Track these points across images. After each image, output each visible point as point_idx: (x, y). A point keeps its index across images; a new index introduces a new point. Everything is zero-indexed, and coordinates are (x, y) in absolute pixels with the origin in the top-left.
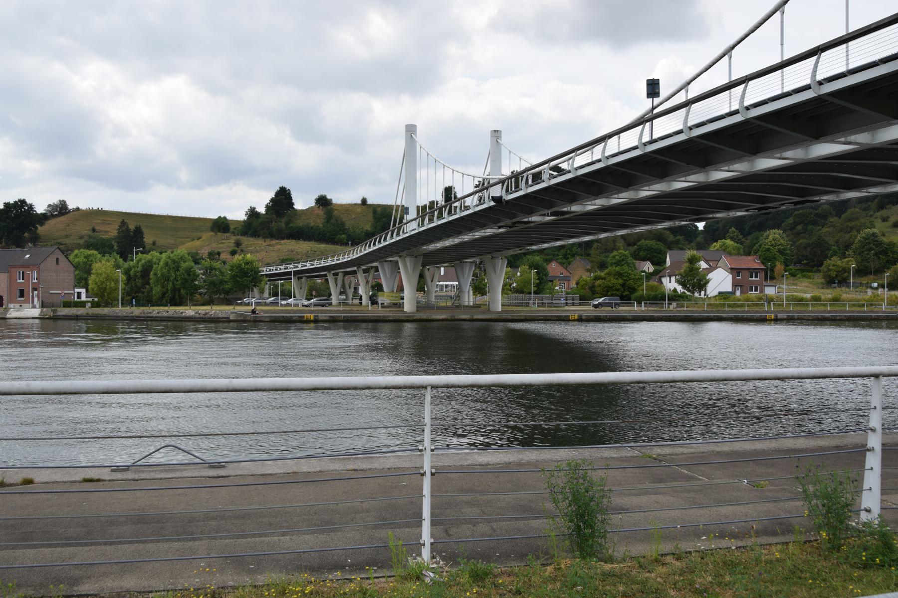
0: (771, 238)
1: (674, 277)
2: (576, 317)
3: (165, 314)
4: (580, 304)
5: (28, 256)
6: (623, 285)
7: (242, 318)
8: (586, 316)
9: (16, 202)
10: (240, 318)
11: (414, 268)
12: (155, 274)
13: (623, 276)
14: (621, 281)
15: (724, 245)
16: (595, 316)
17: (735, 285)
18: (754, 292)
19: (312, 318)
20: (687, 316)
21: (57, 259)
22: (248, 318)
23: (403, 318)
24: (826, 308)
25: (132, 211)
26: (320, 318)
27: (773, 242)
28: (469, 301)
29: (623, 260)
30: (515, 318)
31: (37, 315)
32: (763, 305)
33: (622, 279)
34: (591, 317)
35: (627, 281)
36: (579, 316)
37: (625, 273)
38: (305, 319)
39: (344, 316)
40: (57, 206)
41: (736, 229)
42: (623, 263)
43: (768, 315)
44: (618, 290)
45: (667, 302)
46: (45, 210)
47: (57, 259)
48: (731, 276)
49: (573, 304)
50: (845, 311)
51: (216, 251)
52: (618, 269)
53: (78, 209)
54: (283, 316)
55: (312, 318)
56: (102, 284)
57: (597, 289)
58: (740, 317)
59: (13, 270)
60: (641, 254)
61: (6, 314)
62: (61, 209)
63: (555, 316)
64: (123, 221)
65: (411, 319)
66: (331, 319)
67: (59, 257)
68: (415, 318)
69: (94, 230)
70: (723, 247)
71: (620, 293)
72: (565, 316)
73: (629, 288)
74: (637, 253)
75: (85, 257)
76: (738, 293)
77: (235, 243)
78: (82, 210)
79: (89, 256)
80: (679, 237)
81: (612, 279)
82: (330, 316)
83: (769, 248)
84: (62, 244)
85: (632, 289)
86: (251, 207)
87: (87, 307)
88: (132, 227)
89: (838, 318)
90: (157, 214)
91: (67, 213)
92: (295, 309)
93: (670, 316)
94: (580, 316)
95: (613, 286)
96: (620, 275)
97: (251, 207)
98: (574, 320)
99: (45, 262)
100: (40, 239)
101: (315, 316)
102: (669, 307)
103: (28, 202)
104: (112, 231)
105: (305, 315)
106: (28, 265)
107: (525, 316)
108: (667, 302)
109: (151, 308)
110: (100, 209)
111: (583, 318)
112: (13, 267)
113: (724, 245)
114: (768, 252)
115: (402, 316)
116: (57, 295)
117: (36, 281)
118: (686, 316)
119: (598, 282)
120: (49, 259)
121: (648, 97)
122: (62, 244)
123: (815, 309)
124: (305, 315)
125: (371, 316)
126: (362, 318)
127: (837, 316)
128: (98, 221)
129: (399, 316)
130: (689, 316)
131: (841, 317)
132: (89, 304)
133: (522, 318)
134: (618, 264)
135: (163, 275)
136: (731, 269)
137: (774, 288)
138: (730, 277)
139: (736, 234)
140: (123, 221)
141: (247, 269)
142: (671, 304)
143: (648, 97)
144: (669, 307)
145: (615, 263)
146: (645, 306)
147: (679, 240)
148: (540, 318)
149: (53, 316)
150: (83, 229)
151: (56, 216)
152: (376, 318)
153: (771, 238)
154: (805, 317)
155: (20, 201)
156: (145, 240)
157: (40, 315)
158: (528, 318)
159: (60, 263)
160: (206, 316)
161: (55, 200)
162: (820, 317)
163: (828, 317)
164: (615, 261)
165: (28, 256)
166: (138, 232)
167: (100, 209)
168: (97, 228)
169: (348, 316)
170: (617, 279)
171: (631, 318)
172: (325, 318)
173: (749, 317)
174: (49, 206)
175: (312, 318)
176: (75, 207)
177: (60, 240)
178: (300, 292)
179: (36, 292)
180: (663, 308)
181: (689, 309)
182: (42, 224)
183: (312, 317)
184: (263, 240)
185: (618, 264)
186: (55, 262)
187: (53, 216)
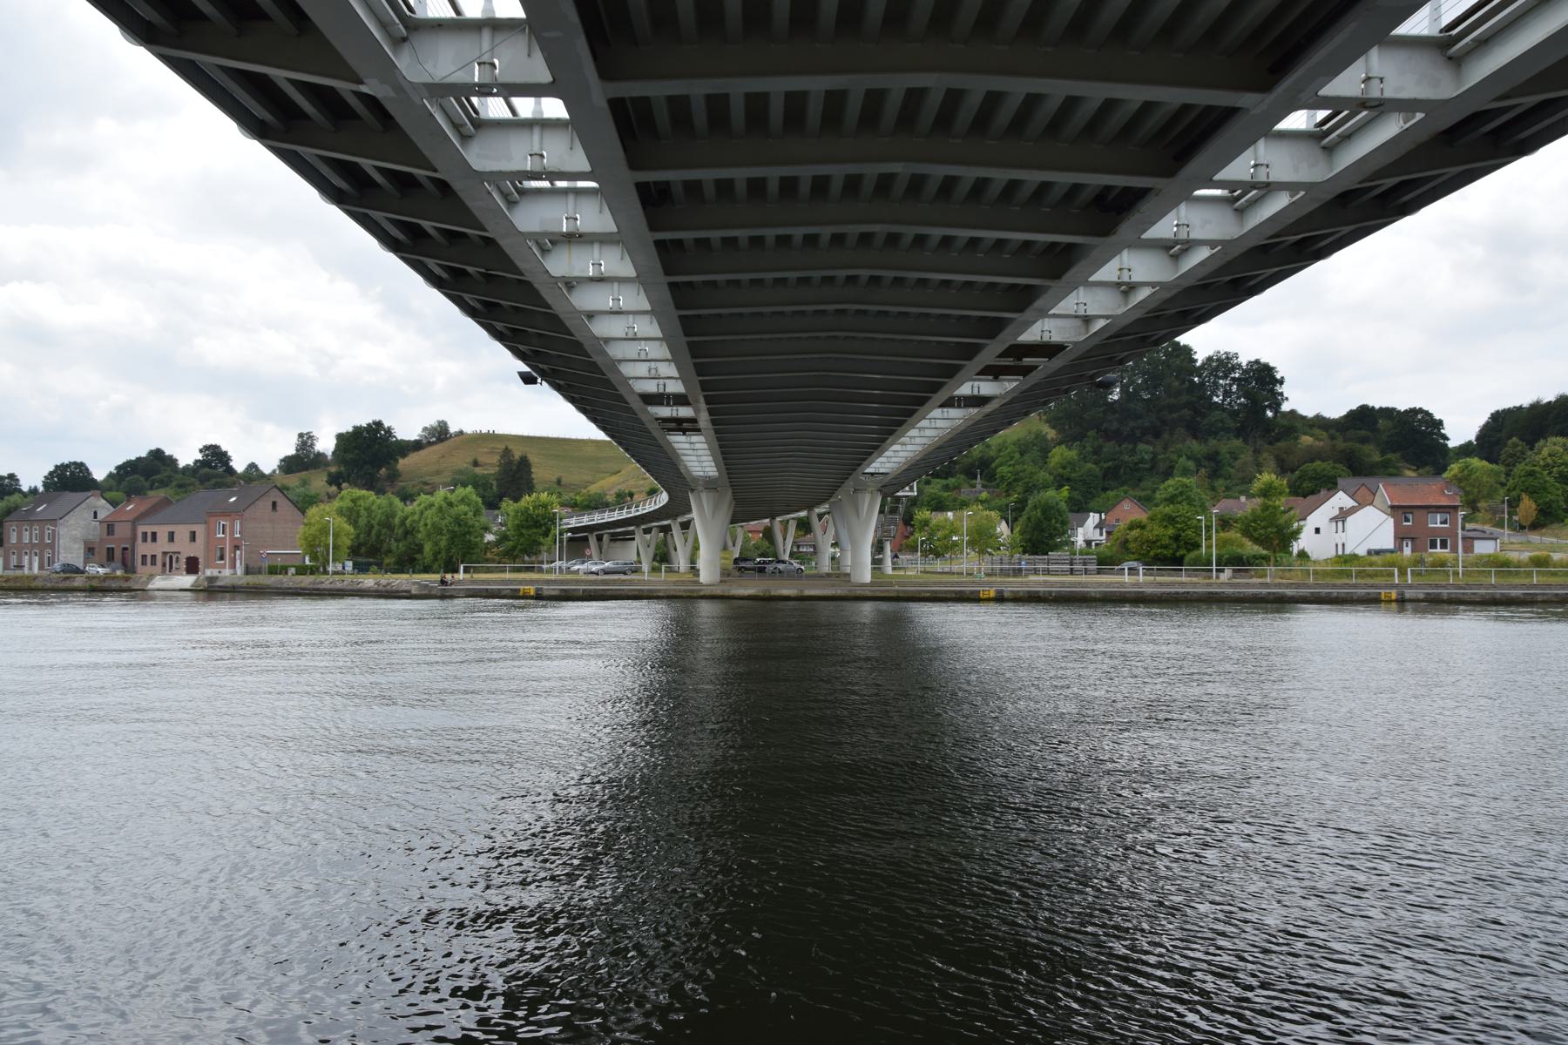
0: (1545, 452)
1: (1097, 515)
2: (992, 594)
4: (1099, 572)
5: (233, 499)
6: (1176, 538)
7: (426, 592)
8: (1011, 591)
9: (369, 425)
10: (423, 592)
11: (716, 508)
12: (426, 525)
13: (1177, 523)
14: (1171, 531)
15: (1467, 467)
16: (1029, 592)
17: (1400, 537)
18: (1439, 550)
19: (532, 593)
20: (1212, 593)
21: (274, 504)
22: (434, 592)
24: (1488, 579)
25: (538, 434)
26: (546, 593)
27: (1549, 460)
29: (1181, 494)
31: (188, 586)
32: (1391, 575)
33: (1174, 527)
34: (1021, 594)
35: (1184, 531)
37: (1181, 516)
38: (521, 593)
39: (584, 590)
40: (435, 429)
41: (1521, 439)
42: (1180, 499)
43: (1383, 591)
44: (1166, 547)
45: (1214, 567)
46: (419, 435)
47: (274, 504)
48: (1391, 521)
49: (1086, 572)
50: (1308, 586)
51: (627, 491)
52: (1168, 509)
53: (461, 433)
54: (1557, 594)
55: (532, 593)
56: (314, 540)
57: (1132, 546)
58: (1323, 595)
59: (212, 519)
60: (1305, 485)
61: (148, 583)
62: (440, 433)
63: (953, 591)
64: (507, 449)
68: (702, 593)
69: (476, 464)
70: (1466, 472)
71: (1171, 551)
72: (972, 592)
73: (1186, 543)
74: (1298, 483)
75: (353, 501)
76: (1407, 551)
78: (467, 434)
79: (359, 498)
80: (1389, 456)
81: (1156, 527)
83: (1533, 471)
84: (428, 484)
85: (1192, 544)
87: (290, 574)
88: (517, 455)
89: (1540, 598)
90: (573, 437)
91: (446, 439)
92: (970, 579)
93: (1177, 593)
95: (1157, 541)
96: (1171, 520)
98: (989, 600)
100: (400, 476)
101: (537, 590)
102: (1218, 577)
103: (386, 425)
104: (491, 465)
105: (521, 587)
106: (229, 512)
107: (898, 591)
109: (414, 576)
111: (1006, 595)
112: (211, 515)
113: (1467, 467)
114: (1531, 479)
115: (679, 590)
117: (238, 536)
118: (1209, 593)
119: (1136, 533)
120: (260, 503)
122: (428, 484)
123: (1502, 581)
124: (521, 587)
127: (1537, 594)
128: (485, 450)
130: (1216, 593)
131: (1545, 598)
132: (293, 570)
133: (891, 595)
134: (1171, 500)
135: (433, 524)
136: (1392, 507)
137: (1494, 542)
138: (1389, 524)
139: (1519, 448)
140: (507, 449)
142: (1223, 571)
144: (1218, 577)
145: (1166, 500)
146: (1144, 574)
147: (1390, 460)
148: (923, 595)
150: (461, 461)
151: (434, 443)
153: (1545, 452)
154: (1466, 598)
155: (375, 423)
156: (533, 476)
157: (192, 586)
158: (901, 595)
159: (278, 508)
160: (389, 588)
161: (431, 421)
162: (1498, 596)
163: (1517, 598)
164: (1168, 496)
165: (233, 499)
166: (524, 463)
168: (480, 459)
169: (590, 590)
170: (1166, 527)
171: (1098, 596)
172: (554, 593)
173: (1343, 595)
174: (425, 429)
175: (532, 593)
176: (457, 430)
177: (427, 479)
178: (646, 552)
179: (238, 552)
180: (1211, 577)
181: (1359, 581)
182: (404, 456)
183: (532, 590)
185: (1171, 500)
186: (271, 507)
187: (430, 444)
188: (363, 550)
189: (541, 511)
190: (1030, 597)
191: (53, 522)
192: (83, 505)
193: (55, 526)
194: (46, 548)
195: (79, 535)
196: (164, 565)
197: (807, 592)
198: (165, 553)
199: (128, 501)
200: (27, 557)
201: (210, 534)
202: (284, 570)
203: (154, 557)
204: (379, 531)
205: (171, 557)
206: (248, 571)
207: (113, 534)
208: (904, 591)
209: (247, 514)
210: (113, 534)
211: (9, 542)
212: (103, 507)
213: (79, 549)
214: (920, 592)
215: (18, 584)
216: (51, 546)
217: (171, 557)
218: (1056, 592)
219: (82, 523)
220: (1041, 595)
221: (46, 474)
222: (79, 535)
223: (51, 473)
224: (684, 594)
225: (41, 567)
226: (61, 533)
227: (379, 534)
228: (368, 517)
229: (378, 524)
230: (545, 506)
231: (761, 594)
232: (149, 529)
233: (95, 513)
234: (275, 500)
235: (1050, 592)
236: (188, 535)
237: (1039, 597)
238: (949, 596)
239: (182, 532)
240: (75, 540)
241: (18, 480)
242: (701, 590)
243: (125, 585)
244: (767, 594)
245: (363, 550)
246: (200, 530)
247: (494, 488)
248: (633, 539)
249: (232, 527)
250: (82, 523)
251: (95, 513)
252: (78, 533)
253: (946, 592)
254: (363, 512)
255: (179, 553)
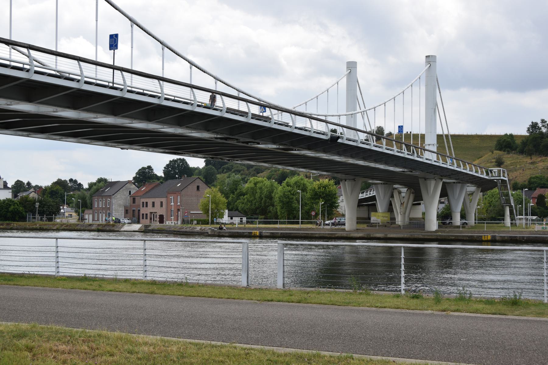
2: (489, 238)
3: (188, 230)
8: (501, 236)
16: (510, 237)
19: (258, 234)
21: (198, 188)
23: (326, 236)
26: (264, 234)
28: (102, 220)
30: (426, 237)
31: (137, 229)
34: (506, 238)
36: (493, 237)
39: (281, 233)
47: (198, 188)
54: (238, 232)
61: (121, 228)
63: (467, 236)
65: (333, 236)
66: (272, 235)
67: (200, 185)
68: (337, 236)
77: (496, 162)
82: (271, 233)
86: (532, 123)
87: (194, 224)
94: (493, 237)
97: (532, 123)
99: (186, 188)
101: (260, 233)
105: (253, 231)
108: (300, 220)
110: (409, 133)
111: (497, 238)
115: (326, 234)
116: (197, 214)
121: (110, 49)
125: (302, 233)
126: (295, 235)
129: (323, 233)
132: (195, 222)
141: (320, 192)
143: (110, 49)
149: (145, 230)
152: (305, 235)
157: (139, 229)
159: (200, 189)
167: (409, 133)
175: (258, 234)
184: (530, 157)
188: (258, 211)
189: (322, 190)
190: (511, 240)
191: (110, 196)
192: (124, 188)
193: (111, 199)
194: (108, 211)
195: (122, 204)
196: (151, 219)
197: (390, 236)
198: (151, 213)
199: (144, 185)
200: (101, 214)
201: (168, 203)
202: (191, 222)
203: (147, 214)
204: (266, 200)
205: (154, 214)
206: (184, 222)
207: (135, 203)
208: (320, 234)
209: (183, 192)
210: (135, 203)
211: (94, 207)
212: (134, 189)
213: (122, 210)
214: (449, 236)
215: (70, 228)
216: (109, 209)
217: (154, 214)
218: (527, 237)
219: (123, 197)
220: (518, 238)
221: (165, 166)
222: (122, 204)
223: (168, 165)
224: (328, 236)
225: (93, 220)
226: (113, 202)
227: (265, 203)
228: (260, 193)
229: (265, 197)
230: (325, 187)
231: (366, 236)
232: (145, 200)
233: (130, 192)
234: (199, 185)
235: (523, 237)
236: (159, 204)
237: (517, 240)
238: (465, 238)
239: (157, 201)
240: (120, 206)
241: (152, 170)
242: (336, 234)
243: (112, 228)
244: (369, 236)
245: (258, 211)
246: (164, 200)
247: (247, 185)
248: (420, 204)
249: (168, 203)
250: (123, 197)
251: (130, 192)
252: (121, 202)
253: (463, 236)
254: (258, 191)
255: (156, 212)
